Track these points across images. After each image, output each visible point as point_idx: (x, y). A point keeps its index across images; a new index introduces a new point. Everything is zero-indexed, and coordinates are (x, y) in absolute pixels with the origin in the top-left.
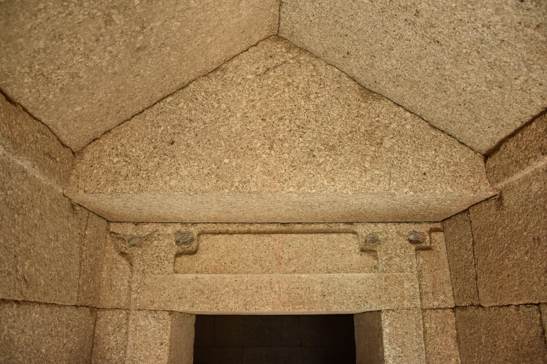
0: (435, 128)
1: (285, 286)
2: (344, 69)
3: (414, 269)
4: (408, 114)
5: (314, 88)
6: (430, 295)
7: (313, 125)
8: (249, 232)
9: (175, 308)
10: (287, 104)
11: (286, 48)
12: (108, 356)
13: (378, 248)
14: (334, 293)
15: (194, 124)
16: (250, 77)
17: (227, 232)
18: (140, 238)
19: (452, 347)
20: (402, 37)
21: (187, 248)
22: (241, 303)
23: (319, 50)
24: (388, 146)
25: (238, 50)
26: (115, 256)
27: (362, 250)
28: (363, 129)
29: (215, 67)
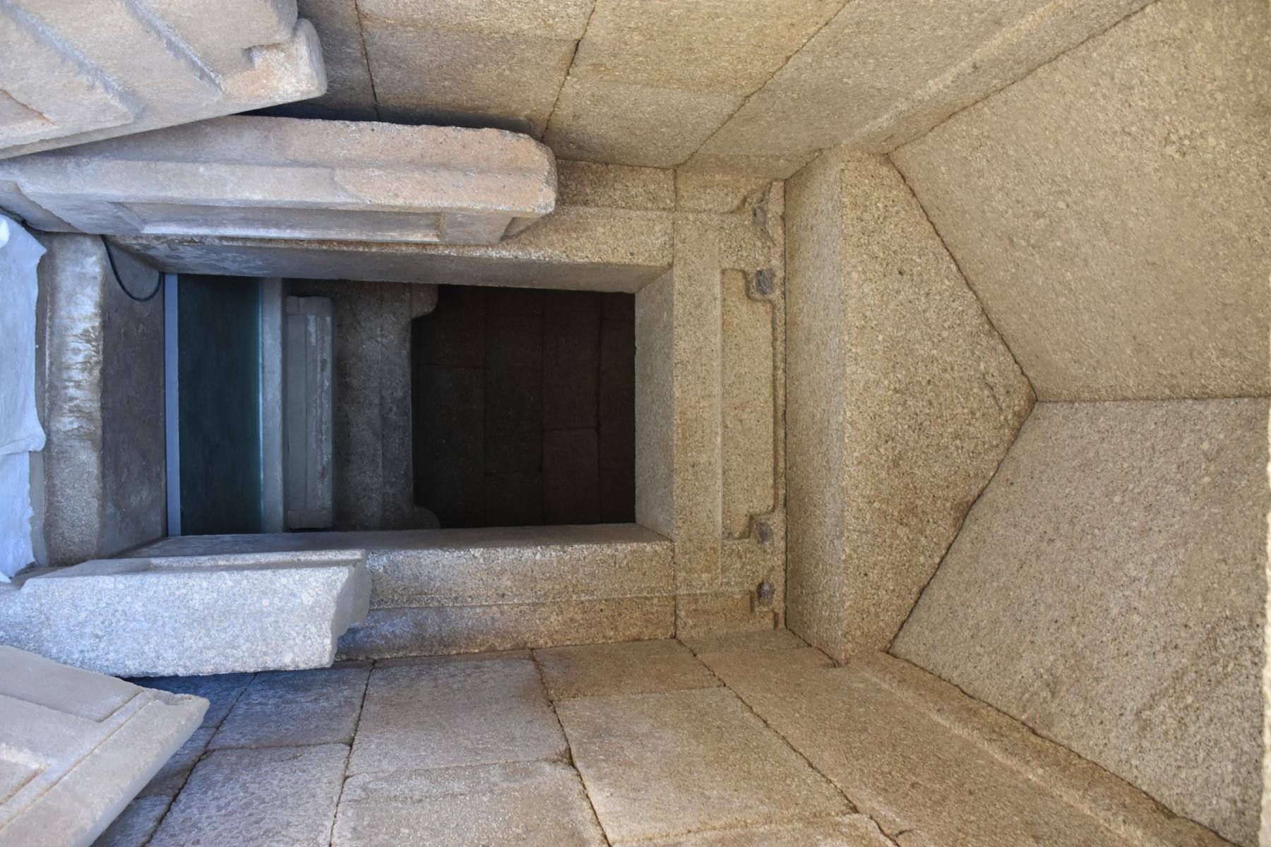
0: (921, 592)
1: (706, 415)
2: (993, 483)
3: (724, 588)
4: (937, 560)
5: (969, 445)
6: (694, 607)
7: (923, 441)
8: (775, 368)
9: (677, 271)
10: (949, 411)
11: (1020, 411)
12: (618, 186)
13: (753, 540)
14: (697, 479)
15: (923, 300)
16: (982, 366)
17: (775, 339)
18: (765, 222)
19: (628, 633)
20: (1027, 532)
21: (758, 284)
22: (685, 358)
23: (1017, 451)
24: (898, 531)
25: (1016, 351)
26: (742, 190)
27: (751, 517)
28: (919, 502)
29: (994, 322)
